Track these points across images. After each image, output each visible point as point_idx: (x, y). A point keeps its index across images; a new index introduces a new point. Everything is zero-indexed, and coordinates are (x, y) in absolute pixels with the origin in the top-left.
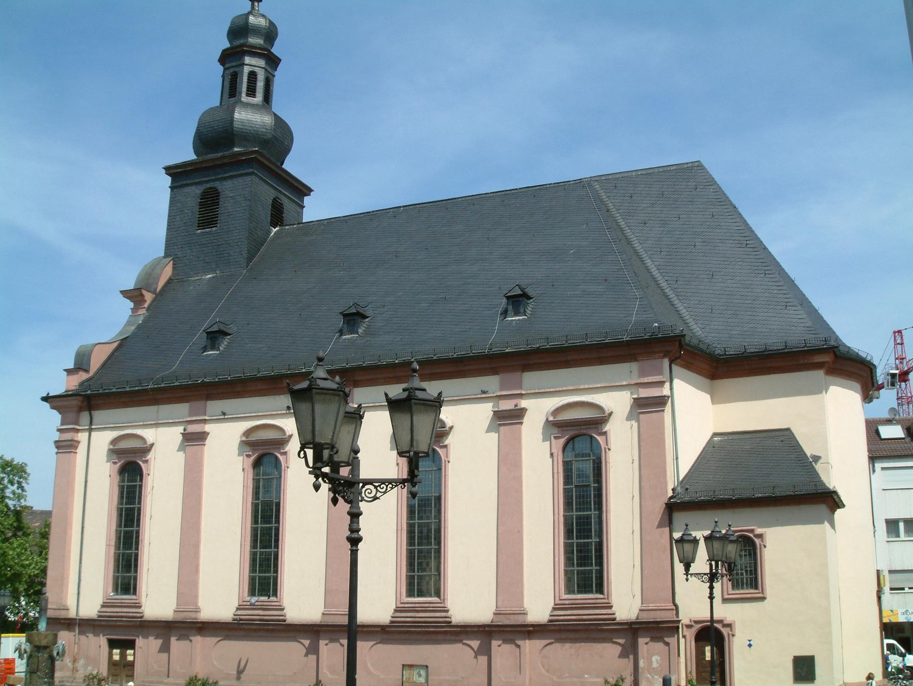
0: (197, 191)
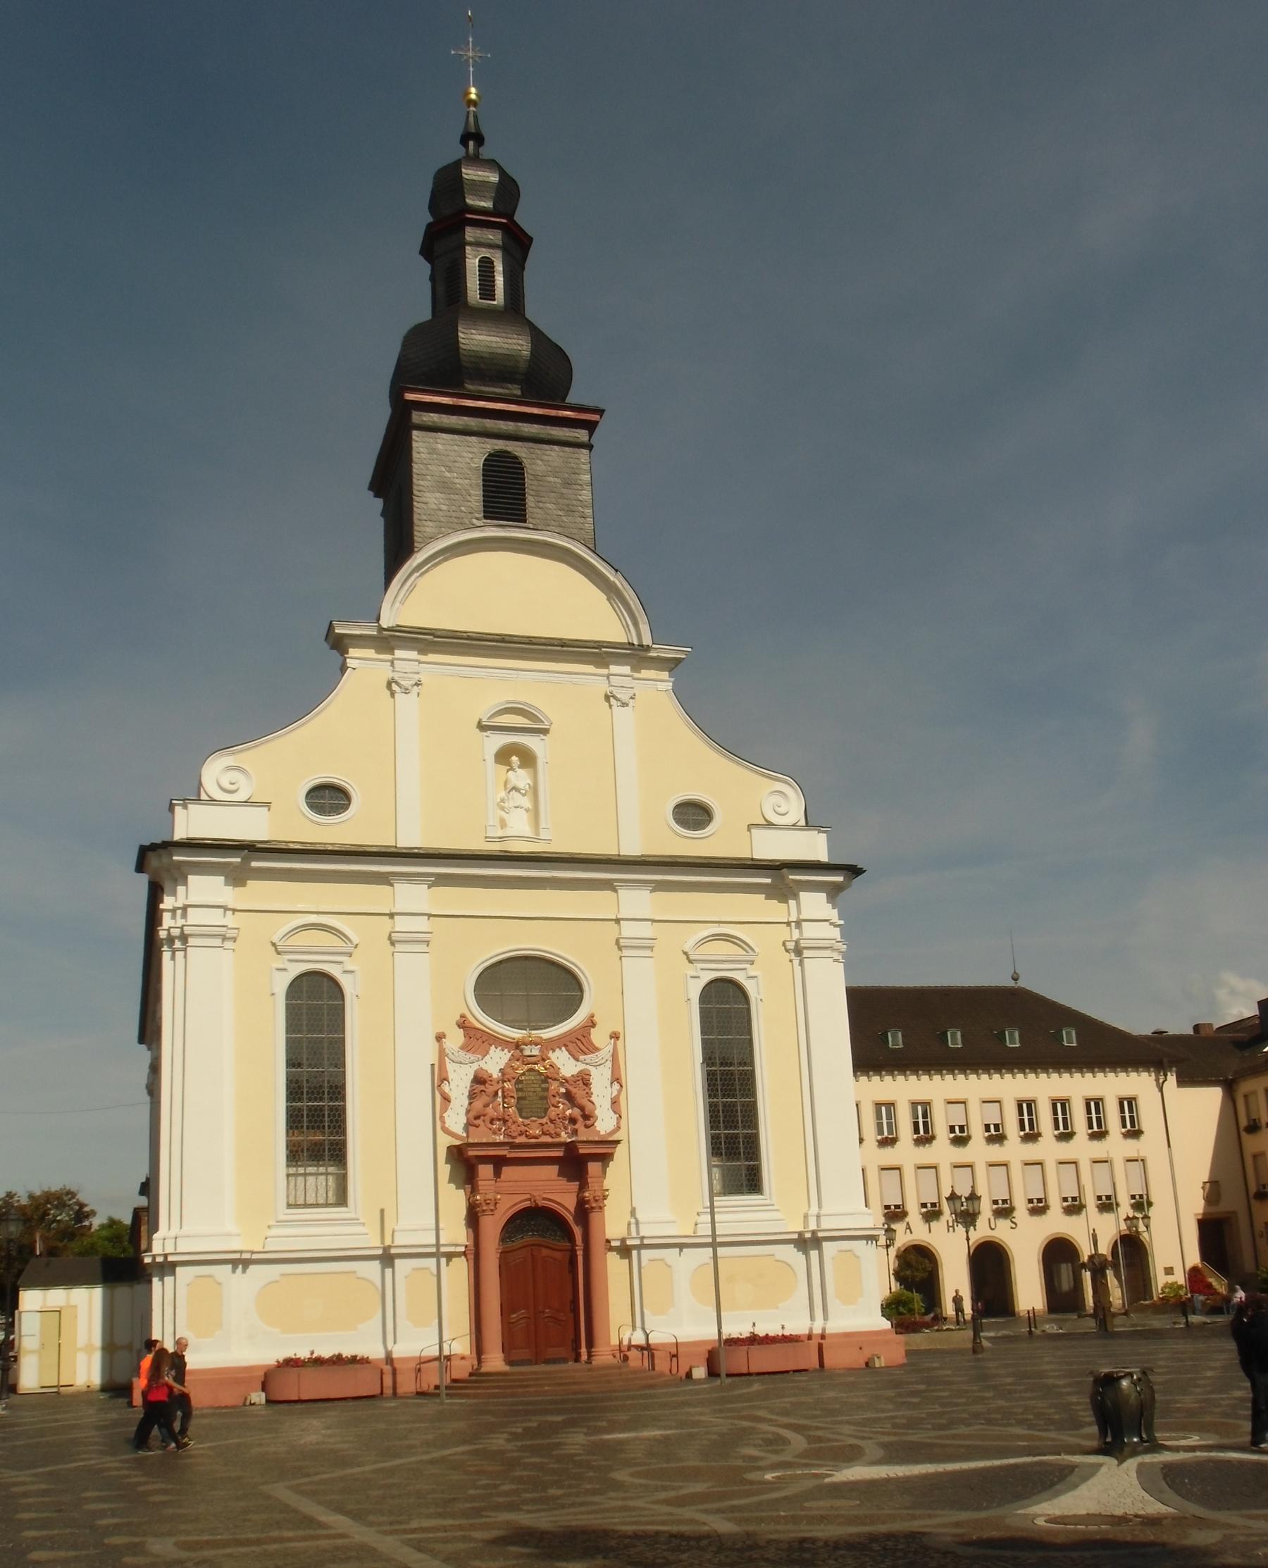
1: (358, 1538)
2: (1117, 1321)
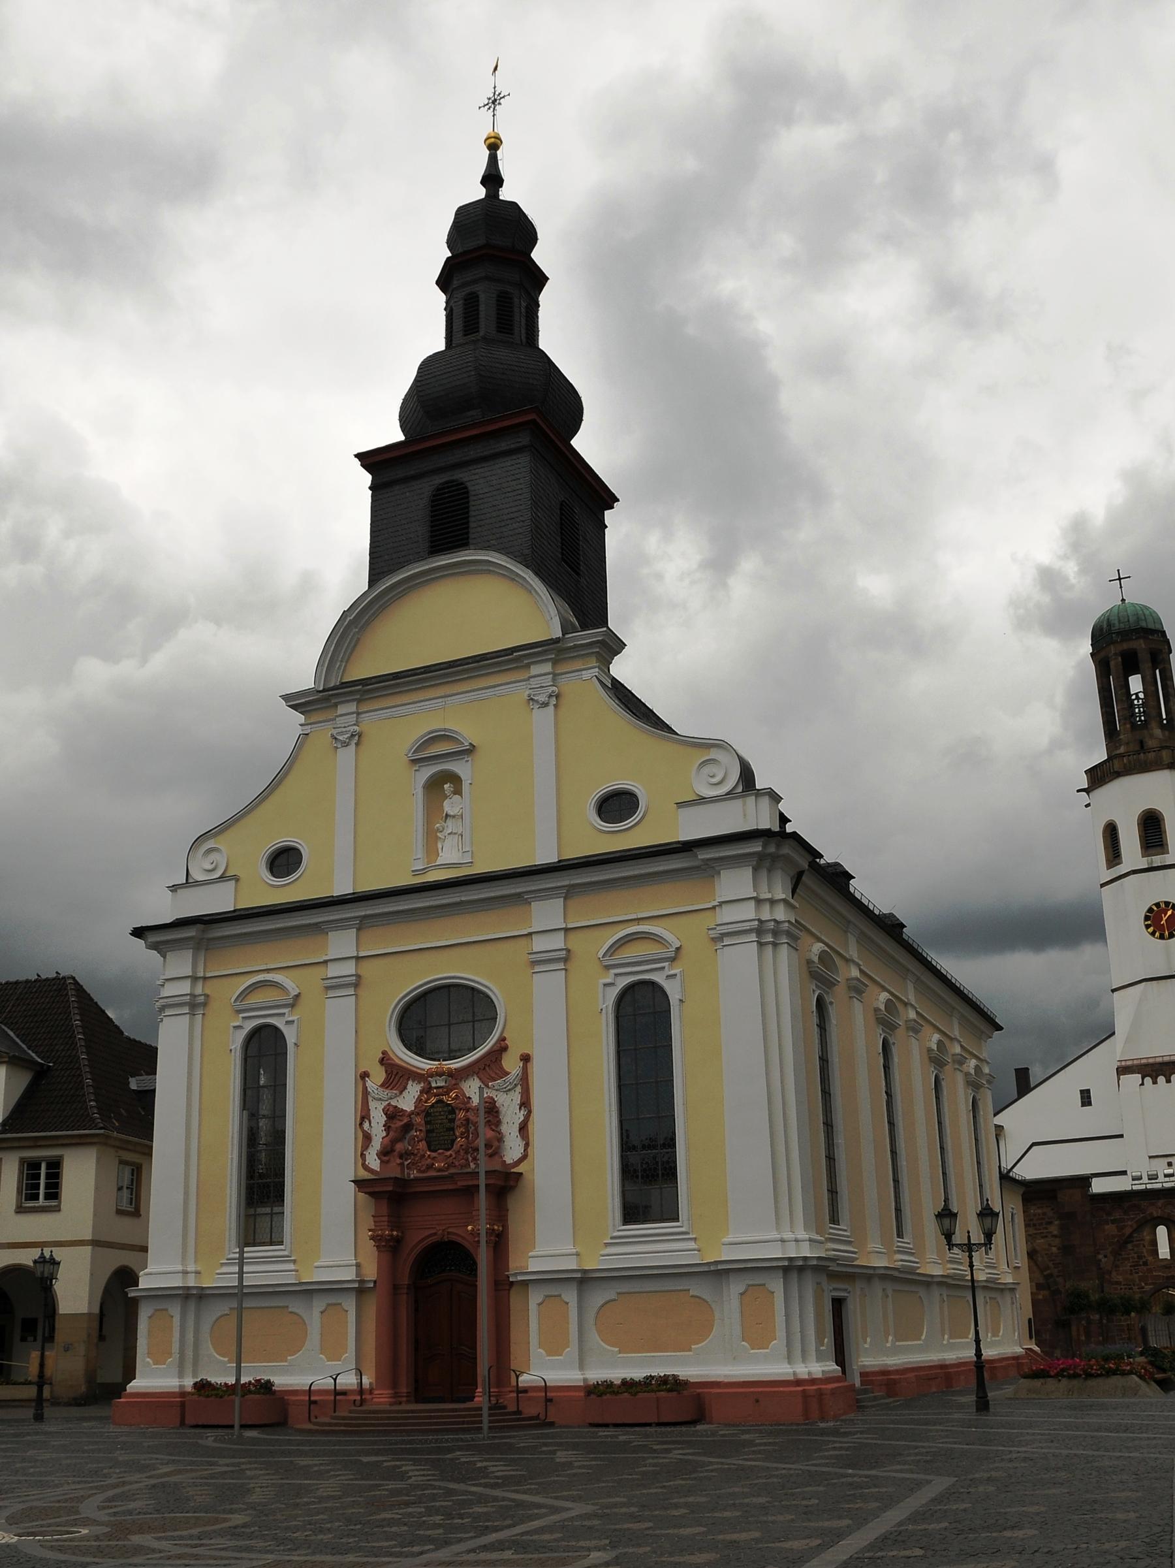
0: (425, 489)
1: (148, 1537)
2: (366, 1381)
